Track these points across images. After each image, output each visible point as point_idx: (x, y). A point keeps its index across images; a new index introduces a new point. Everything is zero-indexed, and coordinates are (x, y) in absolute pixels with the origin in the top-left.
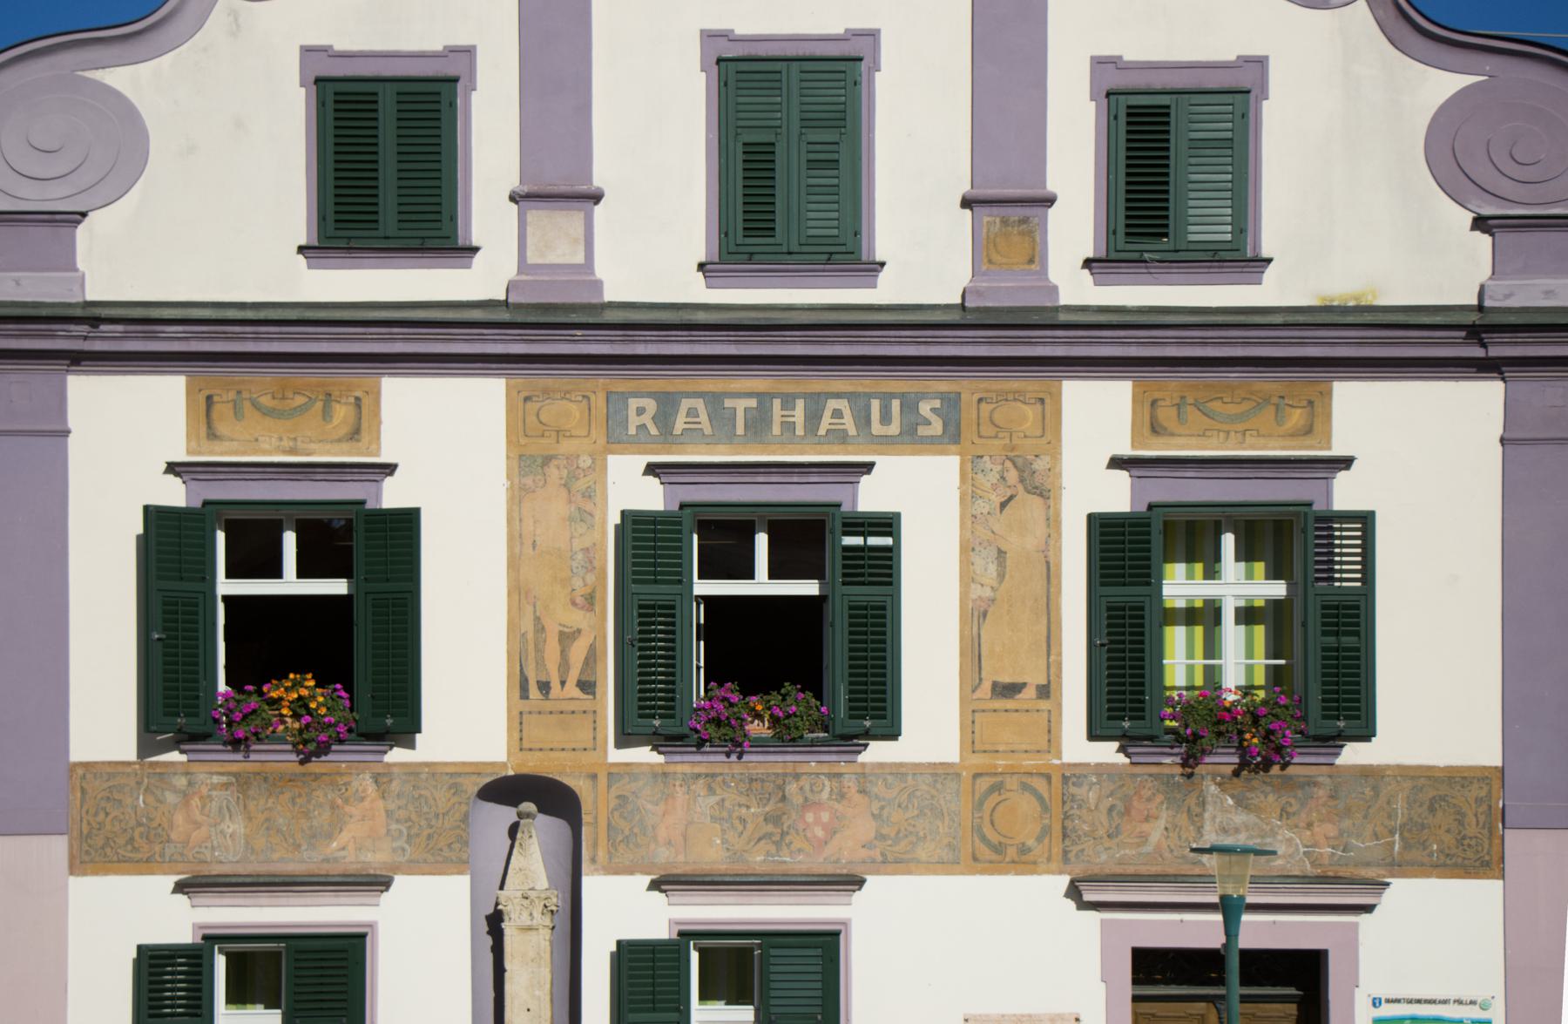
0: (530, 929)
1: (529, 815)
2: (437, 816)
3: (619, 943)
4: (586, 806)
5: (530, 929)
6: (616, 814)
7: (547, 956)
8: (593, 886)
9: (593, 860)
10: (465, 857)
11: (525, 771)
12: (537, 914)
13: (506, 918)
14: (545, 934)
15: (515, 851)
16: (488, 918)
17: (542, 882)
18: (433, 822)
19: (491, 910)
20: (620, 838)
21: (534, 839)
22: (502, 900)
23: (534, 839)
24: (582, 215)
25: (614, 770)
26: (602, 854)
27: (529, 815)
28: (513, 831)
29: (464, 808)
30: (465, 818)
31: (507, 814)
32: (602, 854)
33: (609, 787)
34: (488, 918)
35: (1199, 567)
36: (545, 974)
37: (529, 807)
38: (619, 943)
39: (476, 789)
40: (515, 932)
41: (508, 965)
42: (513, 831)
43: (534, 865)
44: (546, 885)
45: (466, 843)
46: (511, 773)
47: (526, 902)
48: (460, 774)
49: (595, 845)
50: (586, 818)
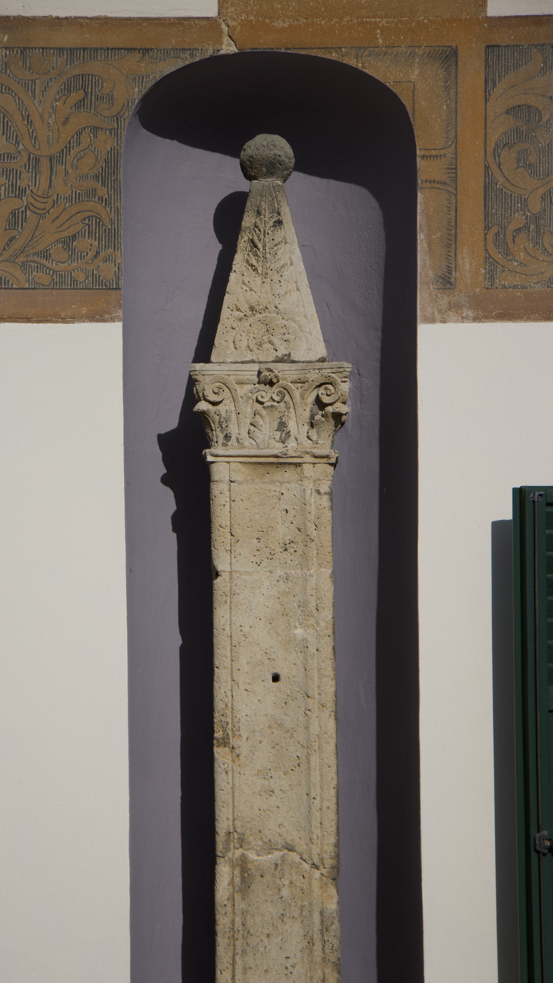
0: (278, 463)
1: (272, 167)
2: (34, 162)
3: (521, 495)
4: (428, 136)
5: (278, 463)
6: (508, 157)
7: (325, 536)
8: (446, 349)
9: (446, 282)
10: (107, 272)
11: (266, 42)
12: (297, 426)
13: (218, 435)
14: (320, 476)
15: (239, 261)
16: (165, 441)
17: (311, 343)
18: (24, 182)
19: (171, 422)
20: (518, 220)
21: (289, 229)
22: (206, 387)
23: (289, 229)
24: (212, 465)
25: (503, 37)
26: (468, 265)
27: (272, 167)
28: (229, 218)
29: (105, 143)
30: (109, 171)
31: (216, 174)
32: (468, 265)
33: (489, 83)
34: (165, 441)
35: (196, 383)
36: (321, 580)
37: (271, 145)
38: (521, 495)
39: (137, 93)
40: (240, 473)
41: (221, 560)
42: (229, 218)
43: (287, 306)
44: (320, 349)
45: (112, 238)
46: (228, 48)
47: (267, 394)
48: (90, 52)
49: (451, 241)
50: (426, 169)
